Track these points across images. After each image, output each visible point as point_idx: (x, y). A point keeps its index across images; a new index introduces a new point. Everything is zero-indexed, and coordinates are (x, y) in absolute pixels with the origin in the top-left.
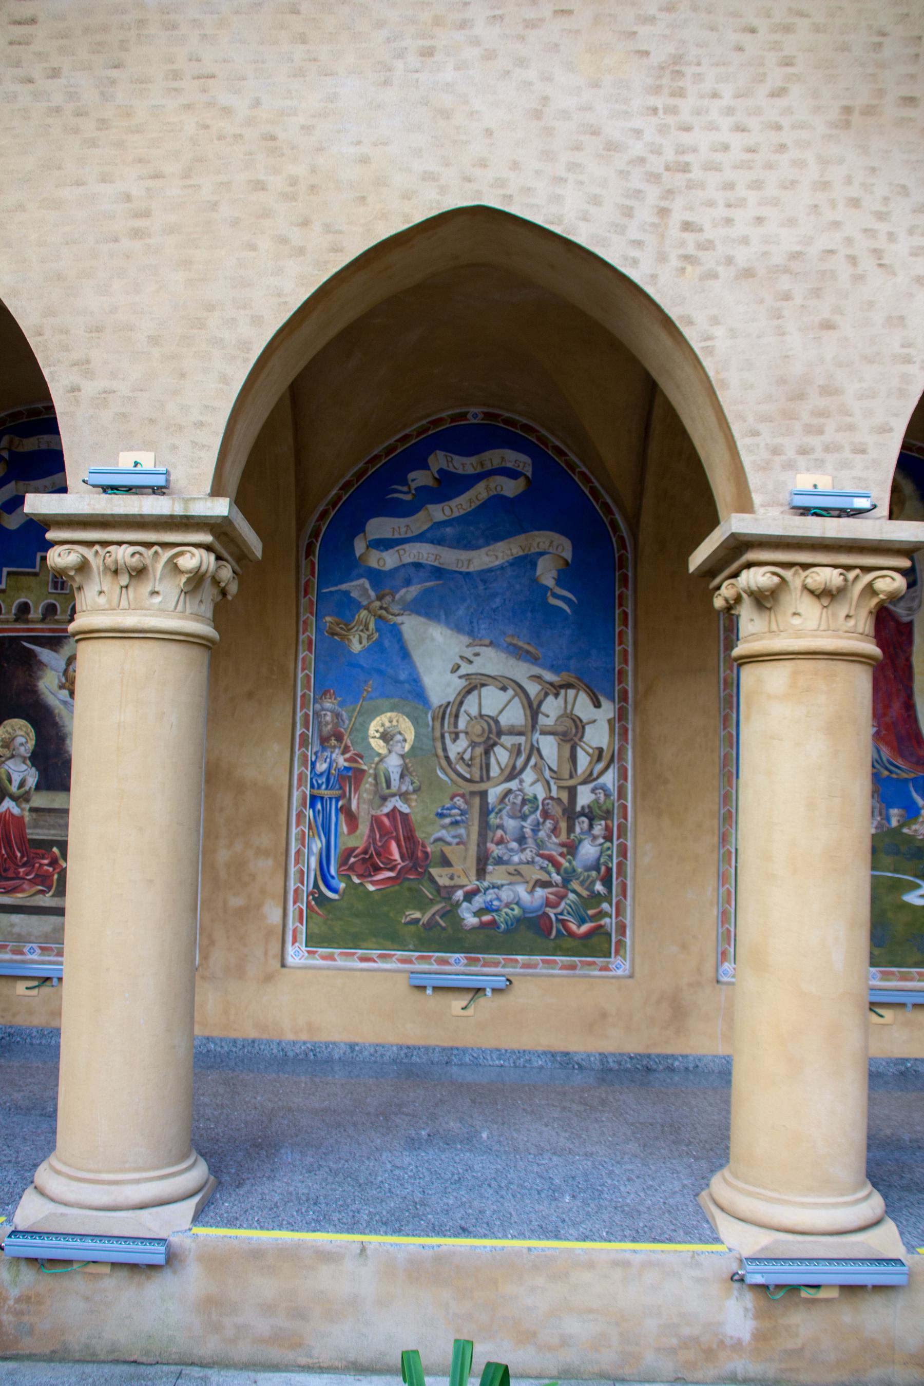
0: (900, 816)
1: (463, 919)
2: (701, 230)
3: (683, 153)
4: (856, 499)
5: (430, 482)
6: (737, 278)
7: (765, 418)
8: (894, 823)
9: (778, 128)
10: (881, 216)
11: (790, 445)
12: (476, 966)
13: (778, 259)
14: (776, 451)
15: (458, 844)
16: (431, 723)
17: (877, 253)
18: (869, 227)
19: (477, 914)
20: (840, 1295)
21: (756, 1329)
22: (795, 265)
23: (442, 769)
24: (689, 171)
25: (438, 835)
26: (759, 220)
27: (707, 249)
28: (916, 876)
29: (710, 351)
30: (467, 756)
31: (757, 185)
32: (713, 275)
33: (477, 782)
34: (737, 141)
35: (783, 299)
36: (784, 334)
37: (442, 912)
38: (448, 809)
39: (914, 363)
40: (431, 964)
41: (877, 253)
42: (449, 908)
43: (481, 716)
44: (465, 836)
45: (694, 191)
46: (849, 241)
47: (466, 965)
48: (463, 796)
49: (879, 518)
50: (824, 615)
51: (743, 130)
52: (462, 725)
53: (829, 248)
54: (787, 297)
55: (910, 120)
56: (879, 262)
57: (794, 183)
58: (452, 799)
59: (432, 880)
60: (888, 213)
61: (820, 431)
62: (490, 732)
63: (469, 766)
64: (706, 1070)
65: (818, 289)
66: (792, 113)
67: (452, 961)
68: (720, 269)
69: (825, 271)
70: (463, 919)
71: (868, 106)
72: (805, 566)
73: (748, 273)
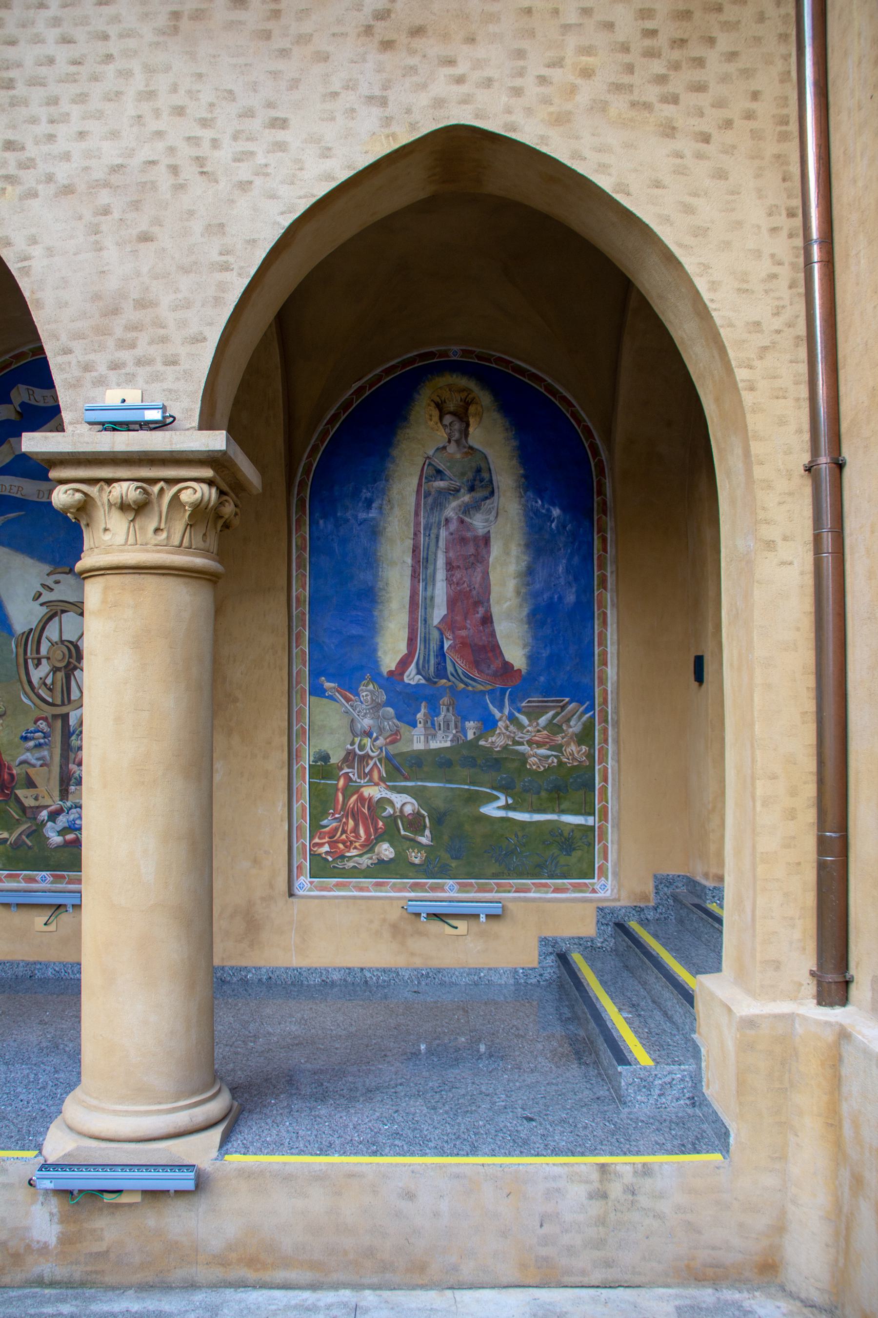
0: (476, 728)
1: (49, 838)
2: (23, 148)
3: (8, 68)
4: (147, 412)
5: (13, 416)
6: (56, 195)
7: (78, 336)
8: (470, 736)
9: (105, 37)
10: (205, 123)
11: (101, 362)
12: (62, 883)
13: (99, 174)
14: (87, 368)
15: (41, 766)
16: (14, 650)
17: (200, 161)
18: (193, 135)
19: (60, 833)
20: (143, 1200)
21: (62, 1233)
22: (115, 179)
23: (26, 693)
24: (14, 88)
25: (23, 758)
26: (82, 135)
27: (28, 168)
28: (493, 788)
29: (26, 271)
30: (49, 681)
31: (82, 98)
32: (33, 194)
33: (58, 706)
34: (62, 54)
35: (101, 214)
36: (101, 249)
37: (28, 832)
38: (31, 732)
39: (232, 270)
40: (19, 882)
41: (200, 161)
42: (34, 828)
43: (62, 642)
44: (48, 758)
45: (16, 108)
46: (171, 150)
47: (52, 883)
48: (45, 719)
49: (188, 429)
50: (132, 528)
51: (69, 42)
52: (44, 651)
53: (150, 159)
54: (106, 211)
55: (240, 22)
56: (201, 170)
57: (119, 94)
58: (35, 722)
59: (18, 800)
60: (213, 120)
61: (133, 346)
62: (70, 656)
63: (50, 690)
64: (279, 982)
65: (137, 201)
66: (120, 21)
67: (39, 878)
68: (40, 187)
69: (145, 183)
70: (49, 838)
71: (197, 10)
72: (109, 482)
73: (68, 190)
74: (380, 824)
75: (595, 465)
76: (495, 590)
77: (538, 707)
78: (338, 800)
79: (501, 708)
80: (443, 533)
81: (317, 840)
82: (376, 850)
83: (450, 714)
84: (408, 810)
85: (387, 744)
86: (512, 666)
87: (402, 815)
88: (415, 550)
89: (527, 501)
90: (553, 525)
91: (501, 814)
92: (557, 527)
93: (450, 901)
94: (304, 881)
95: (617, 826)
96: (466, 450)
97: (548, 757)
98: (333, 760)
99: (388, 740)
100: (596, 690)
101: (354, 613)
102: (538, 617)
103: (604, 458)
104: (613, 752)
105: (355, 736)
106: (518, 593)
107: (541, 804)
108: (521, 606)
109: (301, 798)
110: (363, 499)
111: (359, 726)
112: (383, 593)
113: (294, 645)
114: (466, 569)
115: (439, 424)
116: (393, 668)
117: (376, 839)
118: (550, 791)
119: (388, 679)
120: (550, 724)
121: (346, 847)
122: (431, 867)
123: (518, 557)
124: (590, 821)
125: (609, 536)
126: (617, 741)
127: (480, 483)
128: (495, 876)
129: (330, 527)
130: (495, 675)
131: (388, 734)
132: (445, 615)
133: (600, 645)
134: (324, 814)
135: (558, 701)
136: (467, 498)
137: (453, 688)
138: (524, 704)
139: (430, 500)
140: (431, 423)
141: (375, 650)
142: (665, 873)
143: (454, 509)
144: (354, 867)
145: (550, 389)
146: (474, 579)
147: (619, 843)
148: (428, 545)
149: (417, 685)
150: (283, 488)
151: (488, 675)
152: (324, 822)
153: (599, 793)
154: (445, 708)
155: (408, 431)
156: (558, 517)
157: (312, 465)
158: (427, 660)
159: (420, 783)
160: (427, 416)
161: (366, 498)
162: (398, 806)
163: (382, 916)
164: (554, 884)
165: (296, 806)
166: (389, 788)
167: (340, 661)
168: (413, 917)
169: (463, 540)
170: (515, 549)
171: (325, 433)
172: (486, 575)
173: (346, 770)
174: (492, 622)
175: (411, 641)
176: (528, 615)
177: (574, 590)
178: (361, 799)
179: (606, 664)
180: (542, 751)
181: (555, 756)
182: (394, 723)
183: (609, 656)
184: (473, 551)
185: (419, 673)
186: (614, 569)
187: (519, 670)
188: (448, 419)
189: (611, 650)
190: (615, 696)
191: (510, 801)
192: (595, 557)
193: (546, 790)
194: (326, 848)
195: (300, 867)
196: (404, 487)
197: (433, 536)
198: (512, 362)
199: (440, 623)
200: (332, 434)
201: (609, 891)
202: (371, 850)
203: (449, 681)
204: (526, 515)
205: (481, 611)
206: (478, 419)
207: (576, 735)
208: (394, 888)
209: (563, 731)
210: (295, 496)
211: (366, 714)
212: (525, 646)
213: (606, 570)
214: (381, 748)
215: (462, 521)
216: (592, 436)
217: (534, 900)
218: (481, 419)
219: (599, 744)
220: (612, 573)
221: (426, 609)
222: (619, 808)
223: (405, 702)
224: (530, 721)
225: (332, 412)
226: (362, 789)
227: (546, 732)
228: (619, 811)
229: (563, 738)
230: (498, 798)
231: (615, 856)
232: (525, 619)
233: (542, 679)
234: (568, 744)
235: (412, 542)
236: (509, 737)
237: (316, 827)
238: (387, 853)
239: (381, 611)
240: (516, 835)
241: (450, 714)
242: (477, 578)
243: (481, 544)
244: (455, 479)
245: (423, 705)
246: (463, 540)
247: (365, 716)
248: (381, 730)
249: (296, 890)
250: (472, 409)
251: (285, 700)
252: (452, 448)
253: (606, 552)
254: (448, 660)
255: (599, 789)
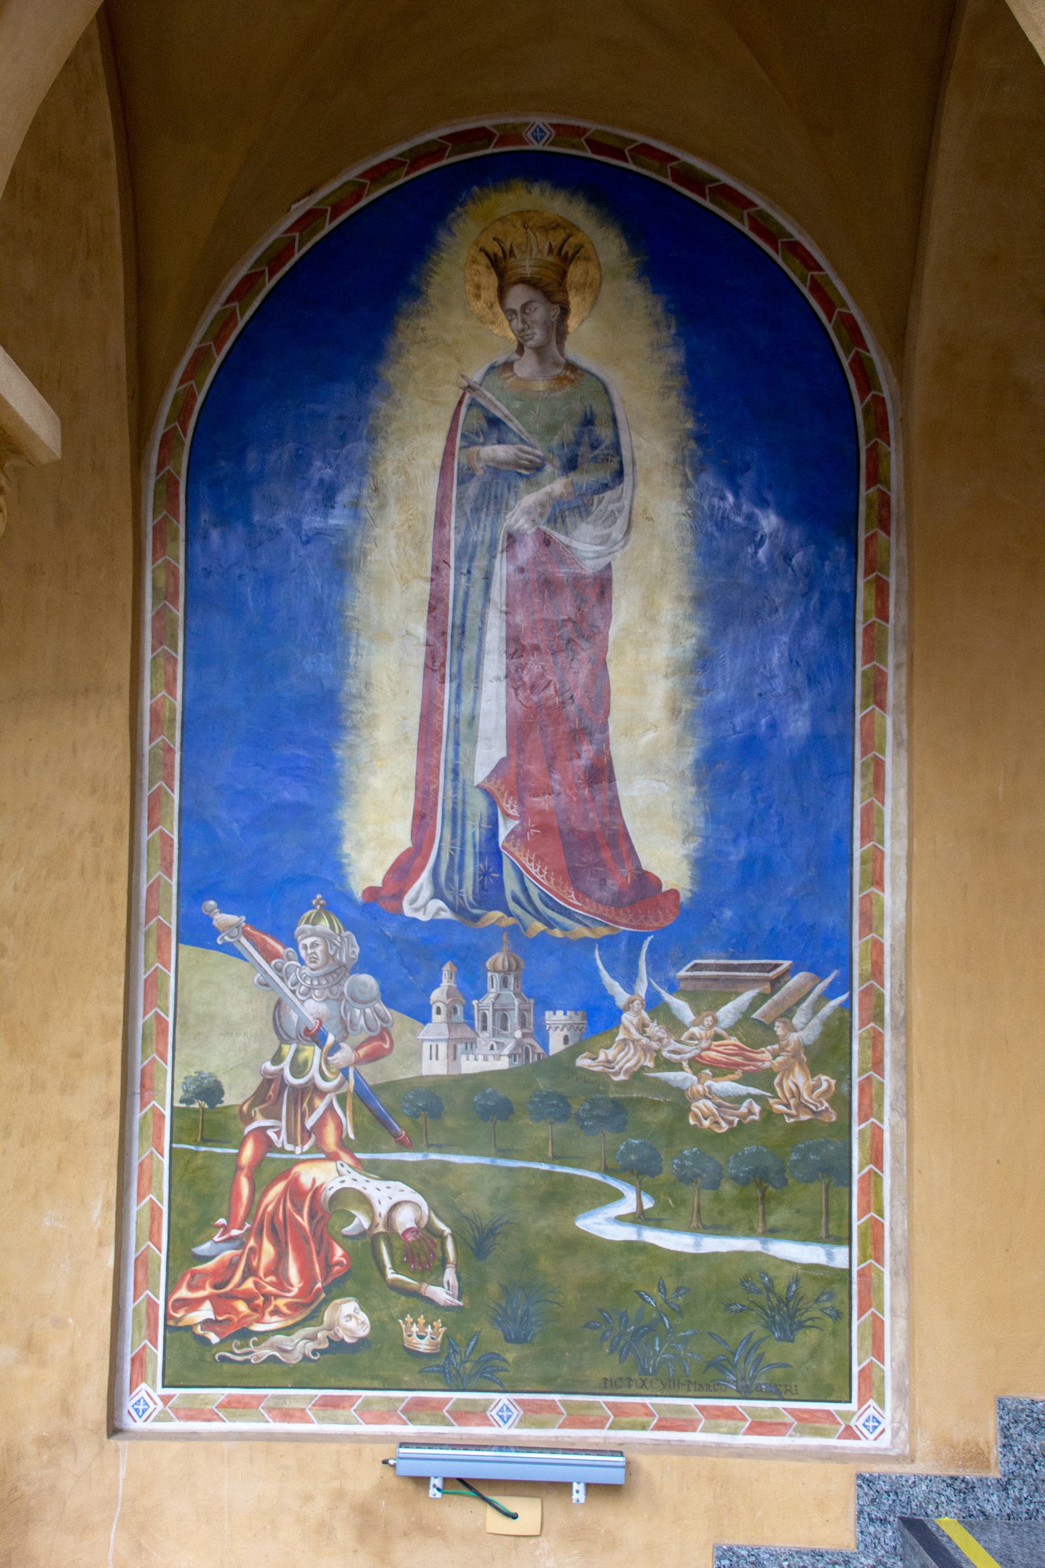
0: (571, 1027)
8: (556, 1045)
28: (607, 1171)
74: (340, 1255)
75: (866, 411)
76: (621, 704)
77: (716, 979)
78: (239, 1195)
79: (629, 983)
80: (502, 569)
81: (183, 1293)
82: (327, 1316)
83: (509, 992)
84: (405, 1219)
85: (358, 1062)
86: (659, 883)
87: (390, 1233)
88: (435, 605)
89: (701, 495)
90: (762, 554)
91: (626, 1233)
92: (770, 558)
93: (501, 1448)
94: (147, 1395)
95: (906, 1271)
96: (559, 371)
97: (739, 1099)
98: (231, 1099)
99: (362, 1052)
100: (856, 942)
101: (288, 751)
102: (721, 768)
103: (886, 394)
104: (895, 1092)
105: (283, 1041)
106: (675, 712)
107: (721, 1213)
108: (680, 742)
109: (149, 1190)
110: (315, 483)
111: (295, 1017)
112: (357, 705)
113: (145, 823)
114: (554, 654)
115: (497, 308)
116: (378, 883)
117: (326, 1289)
118: (743, 1182)
119: (365, 906)
120: (745, 1022)
121: (254, 1308)
122: (457, 1360)
123: (676, 627)
124: (840, 1257)
125: (892, 581)
126: (905, 1067)
127: (591, 451)
128: (609, 1387)
129: (236, 546)
130: (617, 902)
131: (362, 1037)
132: (502, 762)
133: (865, 837)
134: (204, 1226)
135: (763, 968)
136: (558, 486)
137: (516, 932)
138: (683, 973)
139: (472, 489)
140: (478, 306)
141: (336, 840)
142: (1026, 1396)
143: (528, 512)
144: (272, 1359)
145: (763, 225)
146: (570, 677)
147: (911, 1314)
148: (467, 594)
149: (434, 923)
150: (120, 450)
151: (599, 901)
152: (204, 1249)
153: (861, 1189)
154: (497, 978)
155: (423, 322)
156: (774, 534)
157: (194, 397)
158: (457, 866)
159: (434, 1156)
160: (469, 288)
161: (321, 481)
162: (382, 1209)
163: (335, 1484)
164: (752, 1411)
165: (135, 1209)
166: (361, 1166)
167: (251, 862)
168: (411, 1486)
169: (548, 586)
170: (670, 609)
171: (227, 320)
172: (600, 667)
173: (260, 1122)
174: (612, 779)
175: (422, 819)
176: (697, 764)
177: (806, 706)
178: (295, 1191)
179: (879, 883)
180: (726, 1086)
181: (756, 1098)
182: (376, 1012)
183: (887, 863)
184: (571, 612)
185: (438, 894)
186: (904, 656)
187: (674, 893)
188: (518, 296)
189: (893, 848)
190: (900, 957)
191: (648, 1204)
192: (859, 629)
193: (735, 1178)
194: (206, 1312)
195: (138, 1360)
196: (411, 458)
197: (477, 574)
198: (674, 158)
199: (489, 778)
200: (241, 323)
201: (887, 1436)
202: (314, 1317)
203: (509, 914)
204: (697, 528)
205: (587, 751)
206: (589, 299)
207: (807, 1049)
208: (369, 1414)
209: (776, 1039)
210: (153, 470)
211: (310, 989)
212: (688, 836)
213: (883, 661)
214: (345, 1071)
215: (547, 541)
216: (860, 341)
217: (703, 1450)
218: (596, 298)
219: (862, 1071)
220: (898, 667)
221: (457, 744)
222: (911, 1229)
223: (403, 962)
224: (697, 1012)
225: (243, 271)
226: (299, 1169)
227: (733, 1040)
228: (910, 1238)
229: (775, 1056)
230: (619, 1196)
231: (902, 1347)
232: (689, 774)
233: (728, 914)
234: (788, 1070)
235: (427, 587)
236: (646, 1049)
237: (183, 1260)
238: (352, 1324)
239: (352, 747)
240: (662, 1288)
241: (509, 992)
242: (580, 674)
243: (591, 594)
244: (533, 440)
245: (447, 968)
246: (548, 586)
247: (308, 993)
248: (346, 1028)
249: (127, 1419)
250: (576, 272)
251: (119, 954)
252: (526, 367)
253: (886, 619)
254: (506, 863)
255: (862, 1179)
